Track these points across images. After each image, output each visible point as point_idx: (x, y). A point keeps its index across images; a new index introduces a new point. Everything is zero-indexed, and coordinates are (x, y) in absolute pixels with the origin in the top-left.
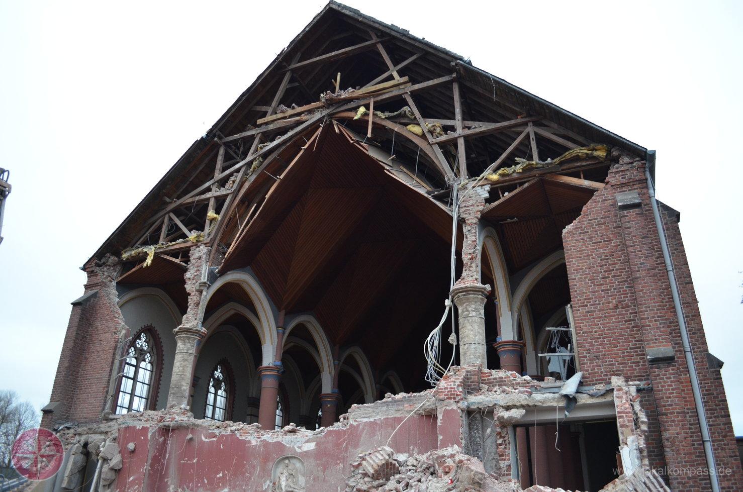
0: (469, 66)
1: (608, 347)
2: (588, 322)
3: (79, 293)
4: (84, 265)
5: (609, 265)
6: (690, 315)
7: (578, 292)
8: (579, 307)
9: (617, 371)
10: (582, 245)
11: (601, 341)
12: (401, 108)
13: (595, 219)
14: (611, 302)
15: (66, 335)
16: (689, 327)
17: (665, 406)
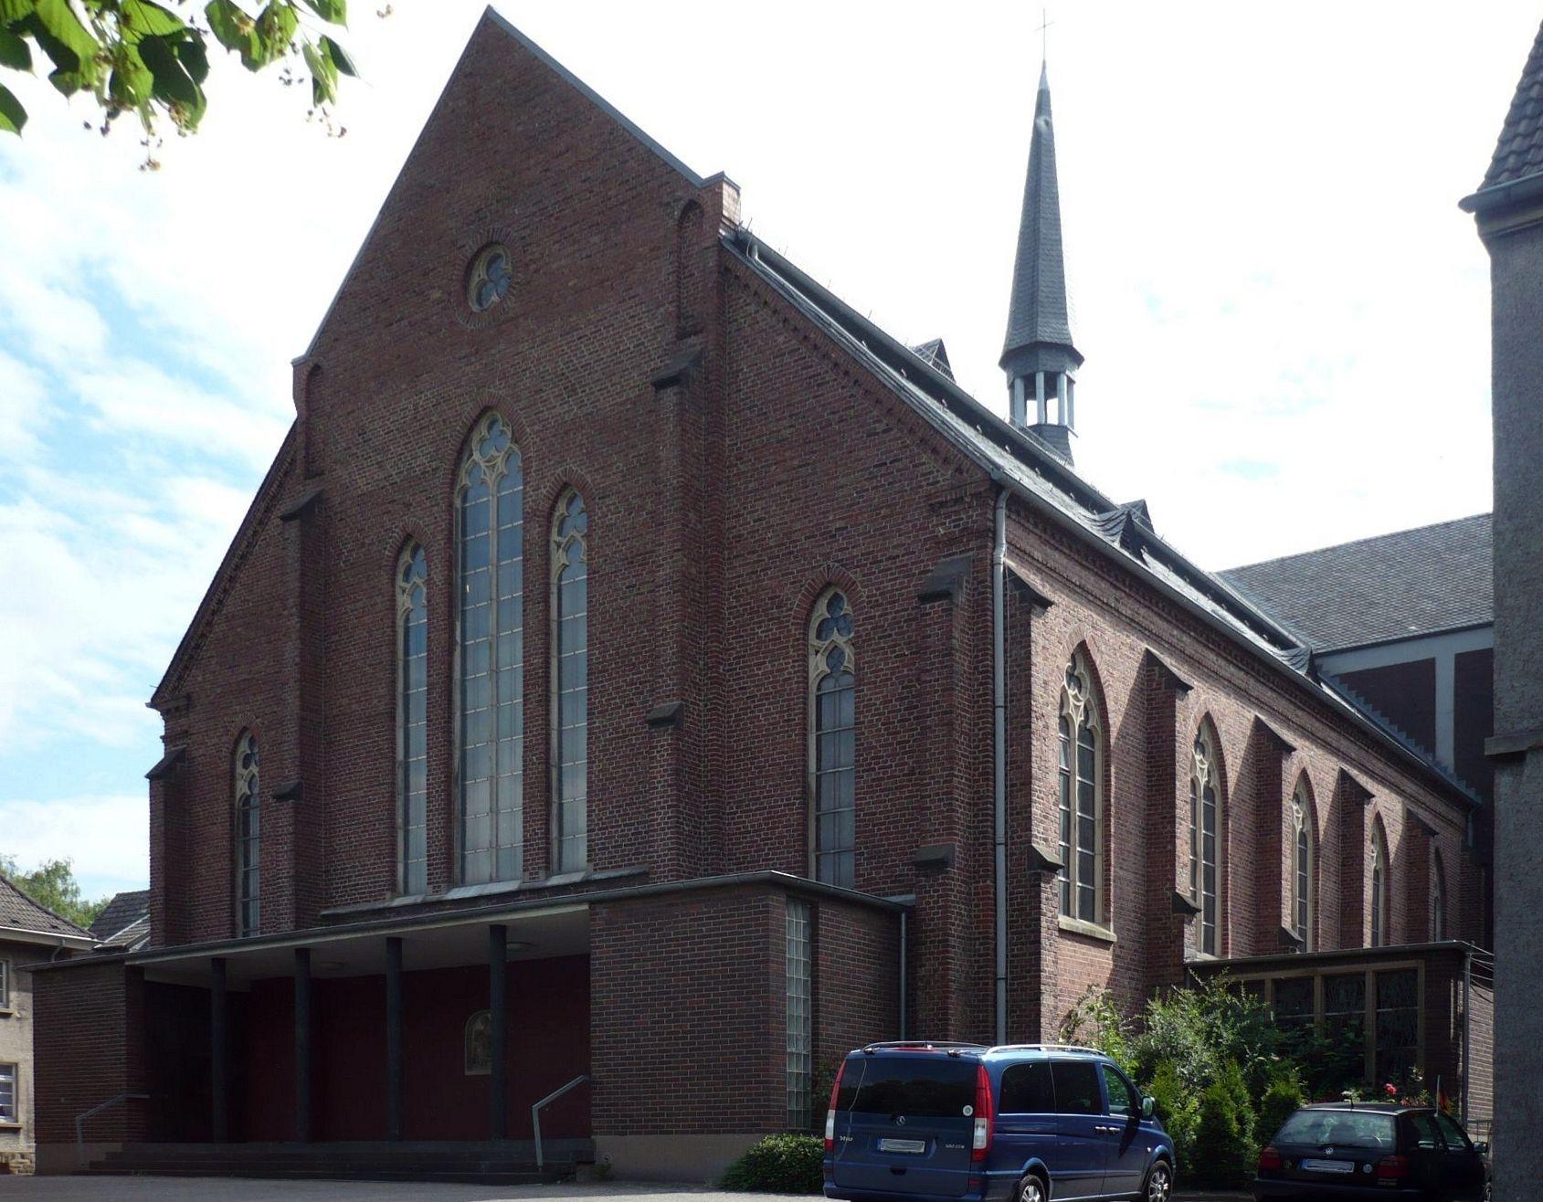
0: (1139, 562)
1: (893, 839)
2: (872, 798)
3: (157, 753)
4: (152, 700)
5: (913, 697)
6: (1018, 782)
7: (865, 745)
8: (863, 771)
9: (900, 876)
10: (880, 660)
11: (885, 829)
12: (149, 69)
13: (902, 610)
14: (906, 763)
15: (151, 832)
16: (1012, 803)
17: (926, 931)
